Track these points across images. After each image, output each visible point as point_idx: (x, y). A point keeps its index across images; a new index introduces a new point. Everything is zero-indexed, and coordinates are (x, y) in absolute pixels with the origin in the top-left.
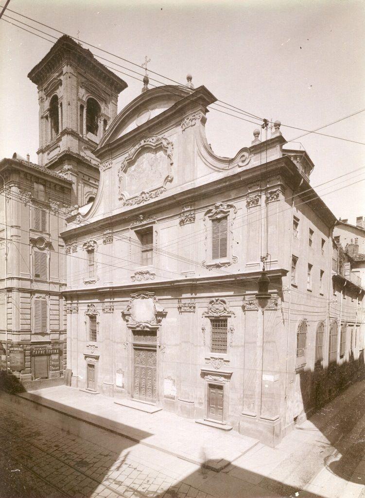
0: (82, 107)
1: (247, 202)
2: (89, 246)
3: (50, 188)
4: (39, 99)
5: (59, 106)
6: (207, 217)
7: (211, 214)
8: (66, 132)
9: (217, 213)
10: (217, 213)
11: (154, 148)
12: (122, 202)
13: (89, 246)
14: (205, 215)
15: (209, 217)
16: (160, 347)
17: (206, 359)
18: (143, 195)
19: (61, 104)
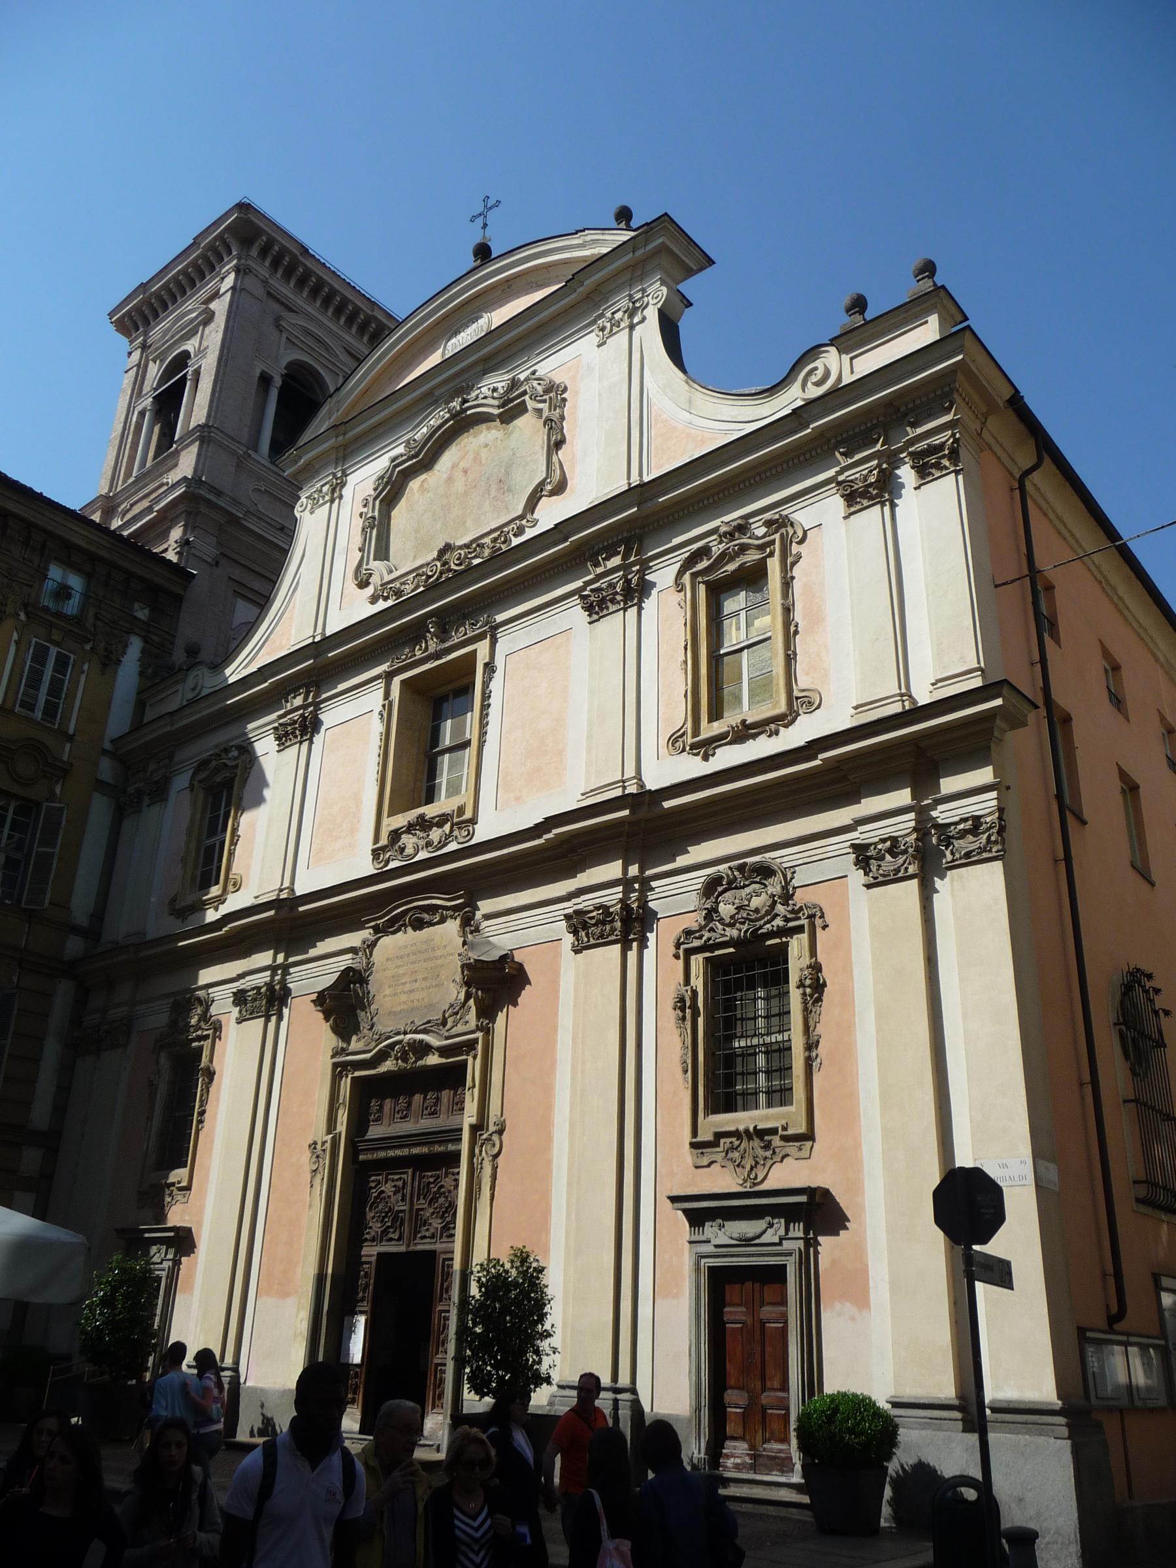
0: (265, 380)
2: (217, 770)
7: (704, 564)
12: (370, 590)
13: (217, 770)
14: (680, 574)
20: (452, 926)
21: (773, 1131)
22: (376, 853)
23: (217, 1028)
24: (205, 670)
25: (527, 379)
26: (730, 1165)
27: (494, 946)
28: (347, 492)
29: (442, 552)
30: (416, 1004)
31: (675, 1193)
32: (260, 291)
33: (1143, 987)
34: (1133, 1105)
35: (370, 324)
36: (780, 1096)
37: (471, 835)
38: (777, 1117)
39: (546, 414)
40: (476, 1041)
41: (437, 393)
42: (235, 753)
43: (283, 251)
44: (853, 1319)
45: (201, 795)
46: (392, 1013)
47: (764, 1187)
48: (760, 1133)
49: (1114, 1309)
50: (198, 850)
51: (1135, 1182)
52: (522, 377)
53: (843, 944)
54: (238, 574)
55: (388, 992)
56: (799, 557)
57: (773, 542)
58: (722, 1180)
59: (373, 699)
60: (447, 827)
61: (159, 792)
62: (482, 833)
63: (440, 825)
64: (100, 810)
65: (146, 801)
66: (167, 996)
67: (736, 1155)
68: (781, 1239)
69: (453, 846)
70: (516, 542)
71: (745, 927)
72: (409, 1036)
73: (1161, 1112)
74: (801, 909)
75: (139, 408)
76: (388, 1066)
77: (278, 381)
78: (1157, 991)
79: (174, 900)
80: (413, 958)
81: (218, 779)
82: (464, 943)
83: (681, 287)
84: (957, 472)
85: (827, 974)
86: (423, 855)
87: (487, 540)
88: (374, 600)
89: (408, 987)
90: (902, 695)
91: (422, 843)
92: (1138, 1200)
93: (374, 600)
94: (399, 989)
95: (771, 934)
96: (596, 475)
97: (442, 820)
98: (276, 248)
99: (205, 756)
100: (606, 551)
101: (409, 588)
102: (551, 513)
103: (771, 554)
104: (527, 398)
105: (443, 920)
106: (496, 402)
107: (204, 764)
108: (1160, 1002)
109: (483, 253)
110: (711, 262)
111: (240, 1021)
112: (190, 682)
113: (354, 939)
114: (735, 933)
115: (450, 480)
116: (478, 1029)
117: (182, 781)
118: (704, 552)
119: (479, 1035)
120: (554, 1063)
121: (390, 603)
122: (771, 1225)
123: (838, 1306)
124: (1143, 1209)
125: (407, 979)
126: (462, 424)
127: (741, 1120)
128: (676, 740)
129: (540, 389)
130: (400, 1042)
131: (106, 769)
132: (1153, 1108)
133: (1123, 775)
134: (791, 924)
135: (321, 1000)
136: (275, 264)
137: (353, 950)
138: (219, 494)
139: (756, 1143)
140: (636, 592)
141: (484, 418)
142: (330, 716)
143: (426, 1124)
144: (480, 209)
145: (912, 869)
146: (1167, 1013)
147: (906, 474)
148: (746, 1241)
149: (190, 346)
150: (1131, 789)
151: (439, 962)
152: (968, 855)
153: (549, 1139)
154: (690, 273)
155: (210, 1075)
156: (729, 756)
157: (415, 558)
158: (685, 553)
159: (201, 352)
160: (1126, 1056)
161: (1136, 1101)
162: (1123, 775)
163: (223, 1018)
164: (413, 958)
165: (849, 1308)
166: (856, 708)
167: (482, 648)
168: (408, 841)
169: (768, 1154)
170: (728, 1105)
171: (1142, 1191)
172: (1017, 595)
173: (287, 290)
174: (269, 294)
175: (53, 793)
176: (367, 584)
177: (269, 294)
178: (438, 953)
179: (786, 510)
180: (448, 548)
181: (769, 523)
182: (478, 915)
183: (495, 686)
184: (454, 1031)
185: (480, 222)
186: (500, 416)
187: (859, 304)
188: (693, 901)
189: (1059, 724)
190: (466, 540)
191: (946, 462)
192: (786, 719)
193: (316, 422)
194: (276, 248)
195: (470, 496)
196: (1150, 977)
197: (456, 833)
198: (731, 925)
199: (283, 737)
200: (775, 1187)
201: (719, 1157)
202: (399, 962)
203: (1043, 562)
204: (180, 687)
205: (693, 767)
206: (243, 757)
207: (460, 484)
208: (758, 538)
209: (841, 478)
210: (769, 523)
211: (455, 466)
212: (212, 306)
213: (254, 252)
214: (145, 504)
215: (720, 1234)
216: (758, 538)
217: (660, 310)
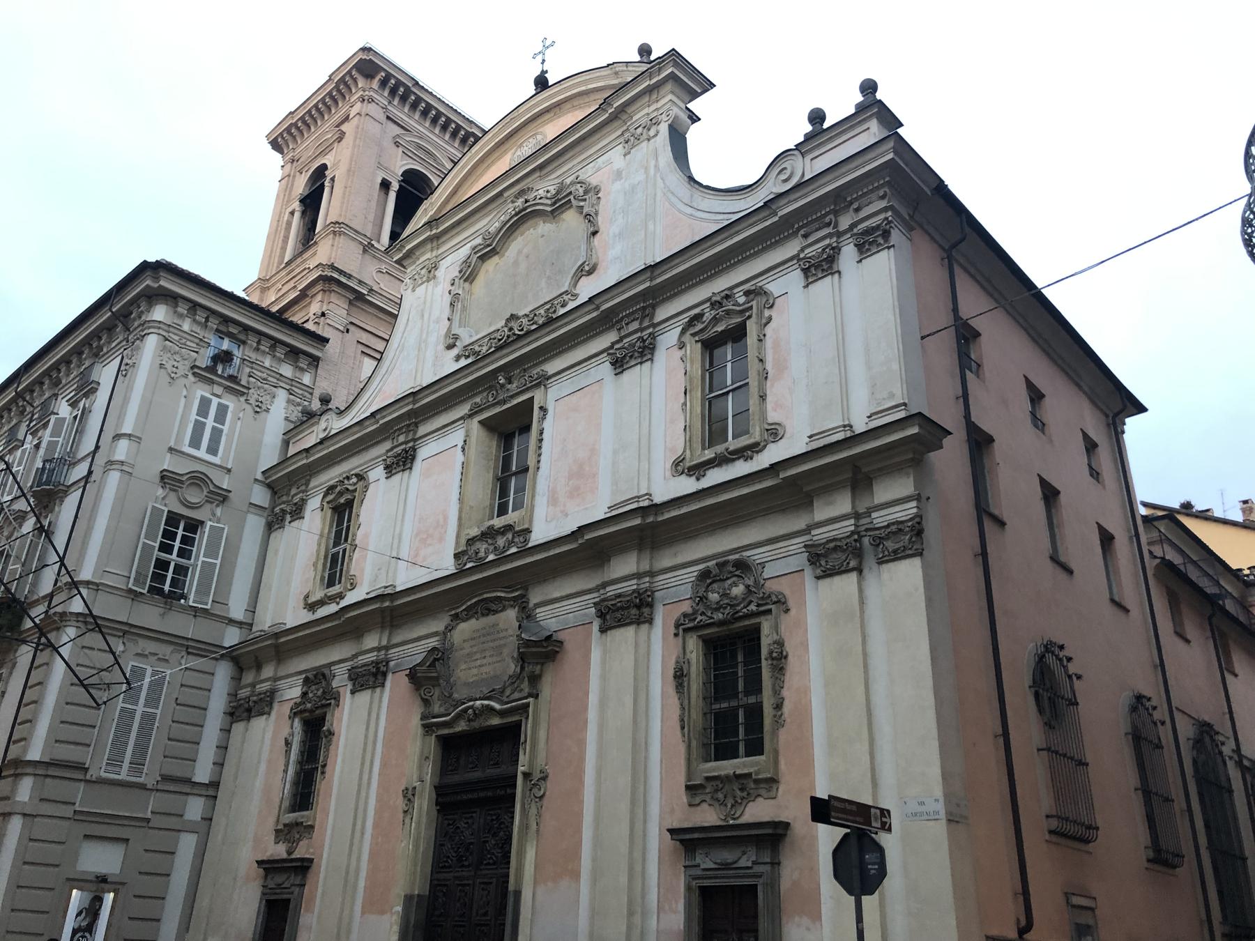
0: (385, 185)
1: (803, 270)
2: (341, 494)
3: (257, 349)
4: (676, 635)
5: (327, 184)
6: (687, 338)
7: (700, 326)
8: (338, 228)
9: (715, 320)
10: (715, 320)
11: (549, 209)
12: (455, 351)
13: (341, 494)
14: (683, 332)
15: (693, 335)
16: (922, 803)
17: (146, 851)
18: (512, 324)
19: (333, 179)
20: (511, 615)
21: (749, 775)
22: (457, 556)
23: (337, 698)
24: (334, 416)
25: (572, 183)
26: (717, 804)
27: (543, 628)
28: (440, 273)
29: (508, 320)
30: (484, 676)
31: (676, 825)
32: (381, 116)
33: (1057, 656)
34: (1045, 753)
35: (462, 133)
36: (755, 748)
37: (526, 541)
38: (752, 765)
39: (585, 210)
40: (528, 705)
41: (506, 195)
42: (354, 480)
43: (399, 83)
44: (808, 929)
45: (330, 512)
46: (467, 684)
47: (743, 820)
48: (738, 777)
49: (1023, 923)
50: (326, 557)
51: (1047, 817)
52: (568, 181)
53: (801, 624)
54: (365, 338)
55: (463, 667)
56: (770, 319)
57: (751, 308)
58: (708, 816)
59: (457, 437)
60: (510, 536)
61: (297, 512)
62: (537, 537)
63: (503, 533)
64: (254, 525)
65: (288, 518)
66: (300, 673)
67: (720, 796)
68: (754, 863)
69: (514, 550)
70: (562, 311)
71: (727, 611)
72: (478, 702)
73: (1072, 758)
74: (769, 596)
75: (290, 209)
76: (461, 726)
77: (395, 186)
78: (1069, 659)
79: (307, 597)
80: (483, 639)
81: (342, 501)
82: (520, 627)
83: (691, 106)
84: (889, 248)
85: (789, 648)
86: (491, 557)
87: (542, 311)
88: (458, 358)
89: (479, 662)
90: (845, 426)
91: (492, 548)
92: (1051, 832)
93: (458, 358)
94: (473, 664)
95: (747, 616)
96: (618, 260)
97: (509, 528)
98: (393, 81)
99: (331, 483)
100: (623, 322)
101: (485, 349)
102: (588, 288)
103: (750, 317)
104: (571, 197)
105: (504, 609)
106: (549, 202)
107: (332, 488)
108: (1072, 669)
109: (542, 83)
110: (712, 85)
111: (603, 630)
112: (323, 425)
113: (438, 625)
114: (721, 616)
115: (516, 263)
116: (530, 695)
117: (314, 503)
118: (698, 317)
119: (531, 700)
120: (586, 721)
121: (469, 361)
122: (744, 853)
123: (797, 919)
124: (1054, 838)
125: (478, 656)
126: (523, 218)
127: (727, 767)
128: (677, 465)
129: (581, 191)
130: (471, 707)
131: (260, 496)
132: (1065, 756)
133: (1044, 483)
134: (762, 609)
135: (413, 675)
136: (393, 92)
137: (435, 634)
138: (350, 277)
139: (736, 786)
140: (645, 351)
141: (536, 214)
142: (424, 452)
143: (491, 772)
144: (540, 48)
145: (853, 564)
146: (1079, 677)
147: (849, 252)
148: (726, 866)
149: (328, 160)
150: (1050, 494)
151: (502, 642)
152: (895, 552)
153: (581, 782)
154: (694, 95)
155: (780, 659)
156: (716, 476)
157: (490, 325)
158: (685, 318)
159: (336, 165)
160: (1041, 710)
161: (1048, 749)
162: (1044, 483)
163: (341, 690)
164: (483, 639)
165: (805, 921)
166: (810, 437)
167: (538, 395)
168: (482, 547)
169: (745, 794)
170: (725, 751)
171: (1054, 824)
172: (945, 344)
173: (402, 114)
174: (388, 118)
175: (214, 515)
176: (454, 345)
177: (388, 118)
178: (501, 635)
179: (760, 282)
180: (513, 317)
181: (747, 293)
182: (531, 605)
183: (547, 425)
184: (513, 697)
185: (540, 58)
186: (552, 212)
187: (817, 117)
188: (687, 592)
189: (979, 442)
190: (526, 311)
191: (880, 240)
192: (755, 448)
193: (414, 219)
194: (393, 81)
195: (530, 276)
196: (1062, 647)
197: (516, 540)
198: (717, 609)
199: (390, 470)
200: (751, 820)
201: (708, 798)
202: (473, 643)
203: (965, 312)
204: (315, 428)
205: (688, 485)
206: (361, 483)
207: (523, 266)
208: (739, 305)
209: (802, 256)
210: (747, 293)
211: (520, 252)
212: (343, 128)
213: (375, 84)
214: (291, 284)
215: (706, 861)
216: (739, 305)
217: (670, 126)
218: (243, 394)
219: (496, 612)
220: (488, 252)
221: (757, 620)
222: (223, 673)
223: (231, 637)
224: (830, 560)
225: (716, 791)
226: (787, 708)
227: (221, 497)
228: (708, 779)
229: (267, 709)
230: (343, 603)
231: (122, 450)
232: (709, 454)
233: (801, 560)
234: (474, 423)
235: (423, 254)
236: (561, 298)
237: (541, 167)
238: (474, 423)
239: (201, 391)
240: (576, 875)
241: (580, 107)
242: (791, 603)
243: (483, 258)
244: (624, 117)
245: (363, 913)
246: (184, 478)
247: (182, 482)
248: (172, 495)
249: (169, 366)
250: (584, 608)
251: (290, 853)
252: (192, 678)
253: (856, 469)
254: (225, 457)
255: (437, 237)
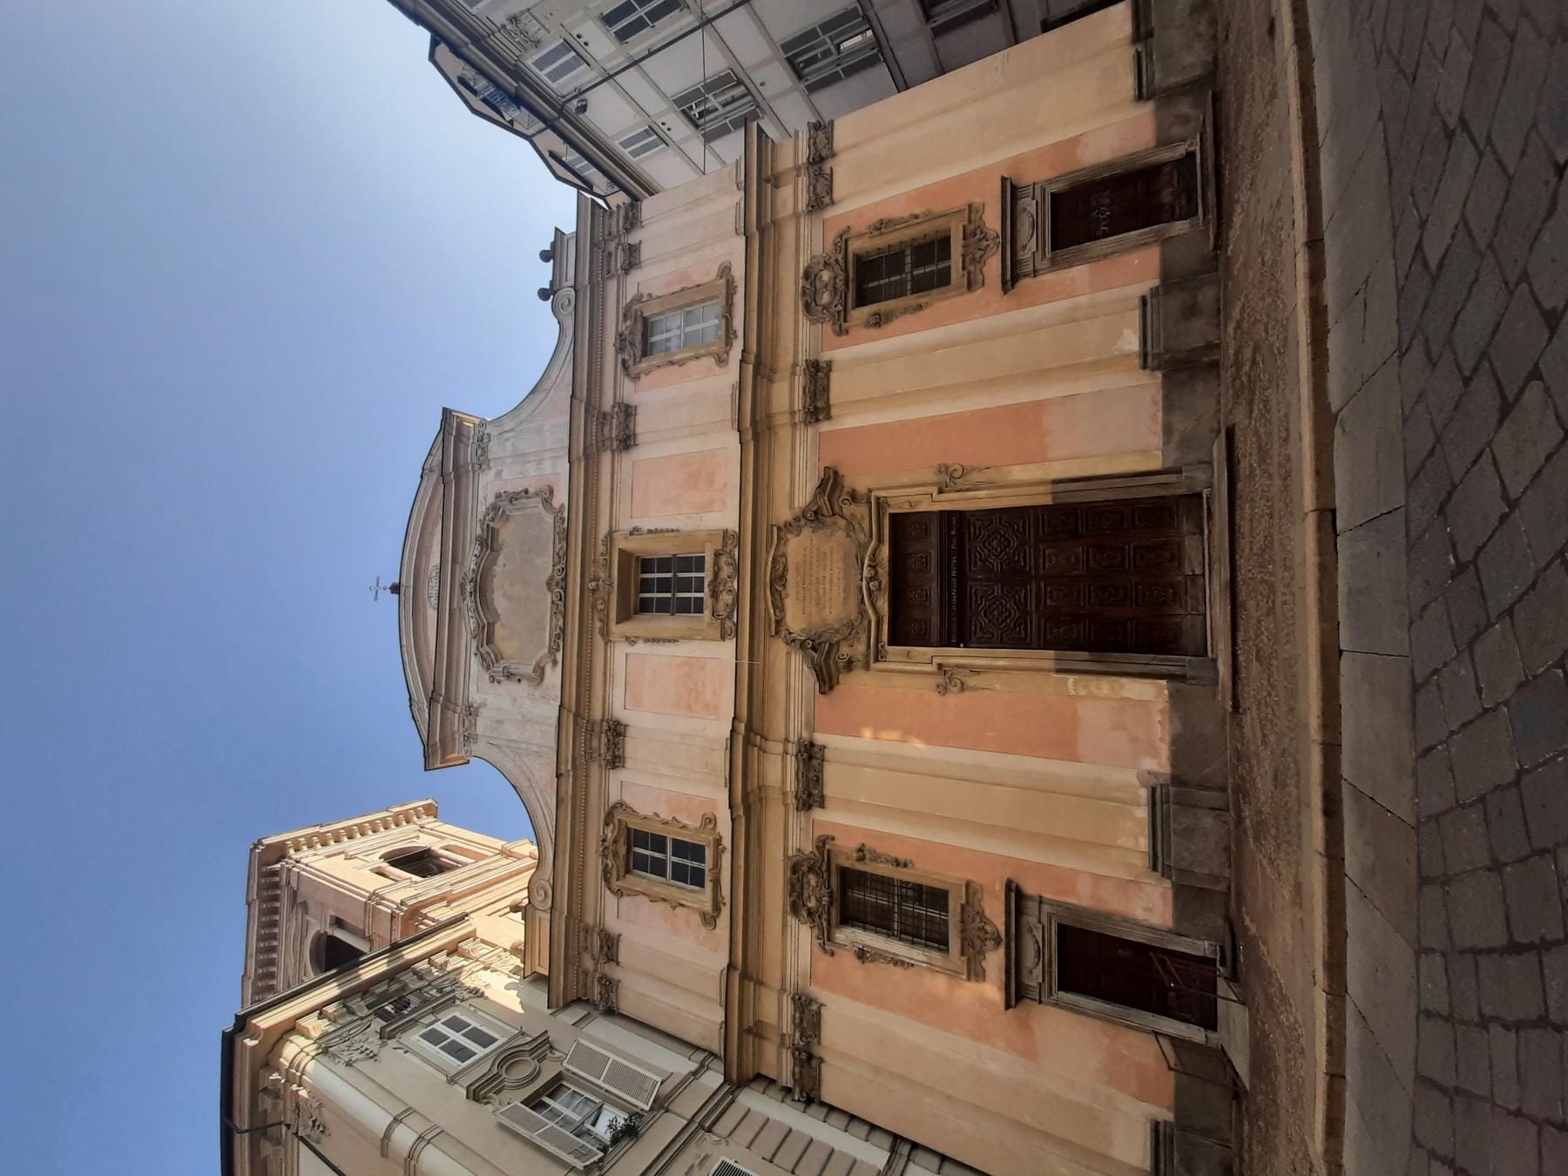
40: (878, 498)
109: (396, 589)
126: (481, 588)
142: (619, 711)
148: (1034, 225)
192: (718, 841)
218: (454, 998)
219: (785, 568)
220: (486, 634)
221: (833, 868)
222: (752, 1100)
223: (713, 1079)
224: (810, 796)
225: (973, 259)
226: (918, 210)
227: (543, 1046)
228: (964, 268)
229: (814, 1007)
230: (727, 842)
231: (404, 1137)
232: (709, 885)
233: (817, 220)
234: (617, 629)
235: (452, 724)
236: (558, 519)
237: (454, 561)
238: (617, 629)
239: (414, 1037)
240: (1039, 406)
241: (432, 534)
242: (844, 226)
243: (490, 641)
244: (463, 470)
245: (1075, 758)
246: (495, 1070)
247: (497, 1076)
248: (506, 1095)
249: (356, 1055)
250: (796, 821)
251: (998, 942)
252: (745, 1134)
253: (749, 1031)
254: (501, 1031)
255: (447, 699)
